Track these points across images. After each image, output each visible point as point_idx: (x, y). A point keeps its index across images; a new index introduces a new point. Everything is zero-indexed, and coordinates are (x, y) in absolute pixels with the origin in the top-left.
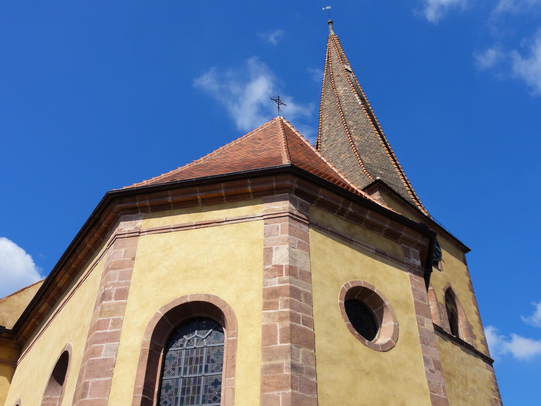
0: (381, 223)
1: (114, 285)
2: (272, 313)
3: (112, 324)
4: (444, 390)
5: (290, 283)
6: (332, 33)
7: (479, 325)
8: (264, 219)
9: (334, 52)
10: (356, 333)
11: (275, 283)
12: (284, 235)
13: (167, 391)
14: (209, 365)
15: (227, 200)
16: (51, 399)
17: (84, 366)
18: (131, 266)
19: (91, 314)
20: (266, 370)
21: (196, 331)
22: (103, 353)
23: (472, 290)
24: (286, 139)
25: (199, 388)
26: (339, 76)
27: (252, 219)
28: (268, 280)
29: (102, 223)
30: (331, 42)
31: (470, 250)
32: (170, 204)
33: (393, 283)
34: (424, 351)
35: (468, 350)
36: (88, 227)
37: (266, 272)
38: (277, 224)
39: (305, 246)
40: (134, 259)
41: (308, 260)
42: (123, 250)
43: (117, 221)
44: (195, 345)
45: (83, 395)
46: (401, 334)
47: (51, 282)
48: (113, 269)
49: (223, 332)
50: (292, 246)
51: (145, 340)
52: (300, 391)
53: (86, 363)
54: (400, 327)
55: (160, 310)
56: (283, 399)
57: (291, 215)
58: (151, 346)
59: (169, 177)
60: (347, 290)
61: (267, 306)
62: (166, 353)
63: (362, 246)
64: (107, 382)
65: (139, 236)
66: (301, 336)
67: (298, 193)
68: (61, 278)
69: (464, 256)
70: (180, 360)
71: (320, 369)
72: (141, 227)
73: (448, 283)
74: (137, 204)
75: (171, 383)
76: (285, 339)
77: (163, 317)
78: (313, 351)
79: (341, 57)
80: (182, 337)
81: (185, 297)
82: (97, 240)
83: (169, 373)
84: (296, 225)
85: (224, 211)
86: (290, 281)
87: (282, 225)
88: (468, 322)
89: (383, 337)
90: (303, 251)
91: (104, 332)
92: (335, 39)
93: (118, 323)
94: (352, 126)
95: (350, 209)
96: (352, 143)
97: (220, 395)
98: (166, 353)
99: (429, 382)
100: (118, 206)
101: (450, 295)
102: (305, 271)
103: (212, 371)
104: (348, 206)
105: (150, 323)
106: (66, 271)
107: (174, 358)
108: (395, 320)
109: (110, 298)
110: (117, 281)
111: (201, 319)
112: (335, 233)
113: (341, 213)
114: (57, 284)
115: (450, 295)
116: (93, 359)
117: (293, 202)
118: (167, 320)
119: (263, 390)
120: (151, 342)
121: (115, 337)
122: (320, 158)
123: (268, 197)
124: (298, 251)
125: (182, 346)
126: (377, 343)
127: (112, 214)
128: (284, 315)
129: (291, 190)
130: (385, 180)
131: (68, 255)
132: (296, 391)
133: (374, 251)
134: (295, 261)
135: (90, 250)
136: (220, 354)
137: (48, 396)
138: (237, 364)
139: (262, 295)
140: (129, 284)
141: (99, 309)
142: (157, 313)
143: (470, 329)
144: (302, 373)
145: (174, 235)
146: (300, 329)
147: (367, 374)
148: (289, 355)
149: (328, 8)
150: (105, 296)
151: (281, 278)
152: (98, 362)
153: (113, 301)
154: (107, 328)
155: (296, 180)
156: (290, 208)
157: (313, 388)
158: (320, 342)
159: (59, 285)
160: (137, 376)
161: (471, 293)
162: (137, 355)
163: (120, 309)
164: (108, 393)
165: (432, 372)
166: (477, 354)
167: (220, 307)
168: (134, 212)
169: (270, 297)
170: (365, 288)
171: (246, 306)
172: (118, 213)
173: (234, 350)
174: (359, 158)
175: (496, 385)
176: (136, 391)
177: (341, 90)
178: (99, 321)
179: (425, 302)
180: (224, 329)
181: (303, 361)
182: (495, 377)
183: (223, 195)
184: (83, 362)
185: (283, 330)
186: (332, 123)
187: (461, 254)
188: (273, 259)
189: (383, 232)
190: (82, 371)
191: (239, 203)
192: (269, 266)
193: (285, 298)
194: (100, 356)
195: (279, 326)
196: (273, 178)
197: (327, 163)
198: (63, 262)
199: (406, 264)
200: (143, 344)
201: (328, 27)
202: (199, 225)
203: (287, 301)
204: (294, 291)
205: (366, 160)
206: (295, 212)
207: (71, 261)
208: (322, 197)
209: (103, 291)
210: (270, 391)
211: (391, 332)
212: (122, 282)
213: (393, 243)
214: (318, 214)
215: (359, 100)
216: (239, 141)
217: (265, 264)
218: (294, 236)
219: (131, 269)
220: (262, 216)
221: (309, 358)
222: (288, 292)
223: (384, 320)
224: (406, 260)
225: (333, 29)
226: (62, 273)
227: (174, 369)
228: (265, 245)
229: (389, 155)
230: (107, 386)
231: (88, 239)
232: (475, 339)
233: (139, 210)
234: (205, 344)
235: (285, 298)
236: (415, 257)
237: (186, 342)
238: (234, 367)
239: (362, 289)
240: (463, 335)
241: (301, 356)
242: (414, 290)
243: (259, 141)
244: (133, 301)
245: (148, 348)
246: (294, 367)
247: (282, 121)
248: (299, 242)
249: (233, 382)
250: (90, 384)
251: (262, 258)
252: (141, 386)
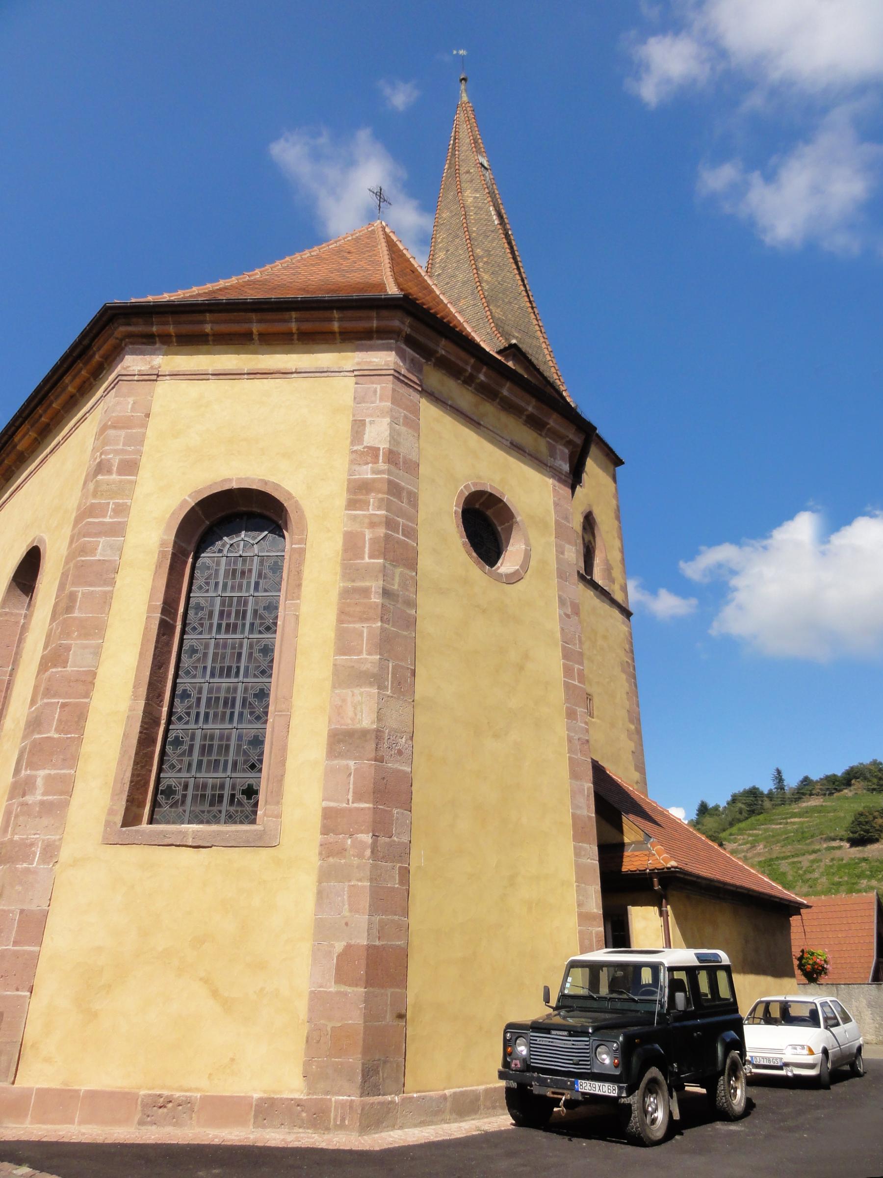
0: (523, 404)
1: (116, 452)
2: (359, 515)
3: (114, 510)
4: (580, 641)
5: (389, 474)
6: (465, 98)
7: (620, 565)
8: (355, 376)
9: (464, 129)
10: (474, 554)
11: (366, 472)
12: (383, 404)
13: (196, 614)
14: (261, 581)
15: (298, 340)
16: (12, 614)
17: (69, 569)
18: (144, 426)
19: (78, 493)
20: (346, 593)
21: (243, 532)
22: (99, 551)
23: (618, 518)
24: (392, 259)
25: (245, 612)
26: (468, 172)
27: (337, 374)
28: (357, 468)
29: (94, 354)
30: (462, 114)
31: (623, 463)
32: (207, 335)
33: (529, 491)
34: (561, 588)
35: (603, 597)
36: (70, 359)
37: (354, 456)
38: (375, 386)
39: (413, 424)
40: (148, 415)
41: (417, 445)
42: (131, 400)
43: (119, 354)
44: (241, 552)
45: (69, 609)
46: (533, 563)
47: (6, 442)
48: (114, 427)
49: (284, 537)
50: (394, 421)
51: (165, 537)
52: (393, 626)
53: (72, 565)
54: (533, 553)
55: (190, 496)
56: (369, 633)
57: (396, 374)
58: (174, 546)
59: (205, 293)
60: (467, 494)
61: (352, 504)
62: (196, 558)
63: (491, 433)
64: (105, 593)
65: (156, 380)
66: (398, 551)
67: (410, 341)
68: (24, 436)
69: (614, 470)
70: (217, 571)
71: (421, 599)
72: (160, 367)
73: (590, 506)
74: (154, 329)
75: (202, 602)
76: (377, 553)
77: (193, 508)
78: (414, 574)
79: (476, 142)
80: (221, 539)
81: (230, 480)
82: (84, 382)
83: (200, 588)
84: (403, 390)
85: (294, 357)
86: (389, 472)
87: (382, 388)
88: (607, 560)
89: (507, 564)
90: (410, 431)
91: (99, 519)
92: (469, 109)
93: (122, 510)
94: (482, 257)
95: (482, 377)
96: (478, 284)
97: (275, 624)
98: (196, 558)
99: (562, 629)
100: (123, 329)
101: (589, 522)
102: (411, 460)
103: (266, 591)
104: (479, 371)
105: (173, 513)
106: (32, 427)
107: (208, 568)
108: (527, 544)
109: (109, 472)
110: (120, 447)
111: (250, 515)
112: (457, 410)
113: (468, 381)
114: (15, 446)
115: (589, 522)
116: (83, 559)
117: (401, 354)
118: (200, 512)
119: (340, 621)
120: (175, 542)
121: (118, 530)
122: (438, 297)
123: (363, 342)
124: (403, 429)
125: (220, 551)
126: (499, 571)
127: (112, 342)
128: (376, 520)
129: (399, 336)
130: (524, 347)
131: (36, 400)
132: (387, 626)
133: (508, 444)
134: (398, 443)
135: (72, 396)
136: (277, 568)
137: (7, 610)
138: (304, 583)
139: (345, 487)
140: (140, 453)
141: (91, 486)
142: (185, 501)
143: (608, 569)
144: (397, 601)
145: (213, 385)
146: (399, 542)
147: (484, 611)
148: (381, 575)
149: (462, 52)
150: (101, 468)
151: (375, 466)
152: (92, 563)
153: (114, 477)
154: (105, 516)
155: (408, 320)
156: (395, 363)
157: (411, 623)
158: (425, 562)
159: (19, 448)
160: (153, 588)
161: (616, 523)
162: (154, 558)
163: (127, 489)
164: (107, 610)
165: (568, 616)
166: (613, 602)
167: (282, 500)
168: (148, 341)
169: (358, 492)
170: (491, 495)
171: (320, 502)
172: (121, 340)
173: (300, 562)
174: (487, 309)
175: (631, 644)
176: (150, 609)
177: (469, 196)
178: (92, 505)
179: (569, 522)
180: (285, 532)
181: (399, 585)
182: (631, 634)
183: (294, 330)
184: (67, 562)
185: (373, 541)
186: (452, 249)
187: (611, 467)
188: (366, 437)
189: (524, 417)
190: (65, 576)
191: (316, 347)
192: (359, 448)
193: (380, 496)
194: (95, 556)
195: (368, 535)
196: (374, 314)
197: (449, 305)
198: (27, 412)
199: (550, 467)
200: (163, 544)
201: (459, 89)
202: (253, 374)
203: (382, 499)
204: (392, 487)
205: (498, 313)
206: (403, 371)
207: (40, 410)
208: (443, 352)
209: (98, 460)
210: (349, 622)
211: (520, 559)
212: (128, 448)
213: (535, 435)
214: (435, 378)
215: (495, 217)
216: (315, 251)
217: (353, 443)
218: (399, 405)
219: (143, 430)
220: (353, 371)
221: (408, 582)
222: (385, 487)
223: (511, 541)
224: (550, 461)
225: (466, 90)
226: (25, 429)
227: (207, 584)
228: (354, 416)
229: (530, 310)
230: (106, 600)
231: (70, 378)
232: (614, 583)
233: (157, 339)
234: (256, 552)
235: (380, 496)
236: (563, 459)
237: (228, 546)
238: (299, 586)
239: (485, 497)
240: (598, 576)
241: (397, 579)
242: (556, 504)
243: (348, 256)
244: (146, 480)
245: (170, 549)
246: (386, 593)
247: (383, 228)
248: (406, 417)
249: (297, 607)
250: (80, 595)
251: (349, 434)
252: (159, 603)
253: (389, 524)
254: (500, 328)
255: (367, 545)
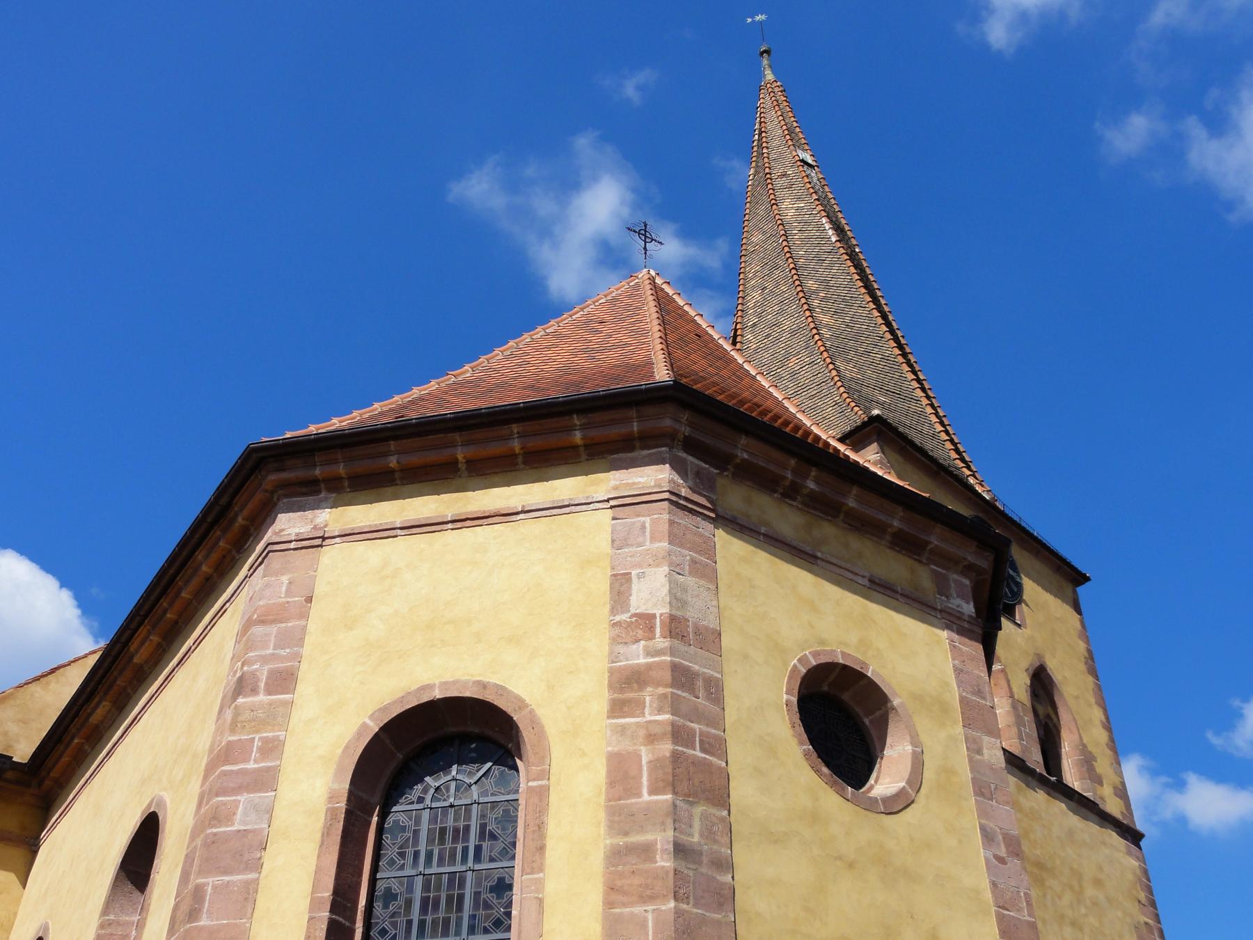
0: (882, 517)
1: (264, 660)
2: (629, 724)
3: (260, 749)
4: (1029, 904)
5: (672, 655)
6: (769, 76)
7: (1109, 752)
8: (612, 507)
9: (773, 120)
10: (825, 770)
11: (637, 655)
12: (657, 545)
13: (386, 906)
14: (485, 845)
15: (525, 463)
16: (118, 923)
17: (195, 848)
18: (305, 615)
19: (211, 726)
20: (616, 856)
21: (455, 767)
22: (238, 816)
23: (1093, 671)
24: (664, 323)
25: (461, 898)
26: (784, 175)
27: (584, 507)
28: (621, 649)
29: (236, 516)
30: (768, 98)
31: (1088, 579)
32: (393, 471)
33: (911, 656)
34: (982, 813)
35: (1084, 810)
36: (204, 526)
37: (617, 630)
38: (642, 519)
39: (706, 570)
40: (309, 599)
41: (715, 603)
42: (285, 579)
43: (270, 511)
44: (452, 800)
45: (193, 914)
46: (929, 774)
47: (119, 653)
48: (262, 622)
49: (517, 770)
50: (676, 570)
51: (336, 786)
52: (696, 905)
53: (199, 841)
54: (926, 758)
55: (371, 717)
56: (656, 923)
57: (674, 498)
58: (349, 800)
59: (390, 410)
60: (804, 671)
61: (618, 708)
62: (383, 816)
63: (838, 570)
64: (247, 883)
65: (321, 546)
66: (697, 777)
67: (691, 446)
68: (142, 643)
69: (1075, 592)
70: (416, 833)
71: (741, 855)
72: (326, 526)
73: (1039, 656)
74: (317, 472)
75: (396, 887)
76: (661, 784)
77: (376, 734)
78: (725, 813)
79: (791, 131)
80: (421, 780)
81: (429, 687)
82: (224, 557)
83: (392, 863)
84: (686, 520)
85: (519, 489)
86: (673, 651)
87: (653, 522)
88: (1084, 746)
89: (886, 780)
90: (702, 582)
91: (241, 768)
92: (776, 90)
93: (273, 748)
94: (816, 292)
95: (811, 485)
96: (815, 331)
97: (509, 914)
98: (383, 816)
99: (994, 885)
100: (273, 477)
101: (1042, 684)
102: (707, 628)
103: (492, 860)
104: (806, 477)
105: (347, 747)
107: (403, 829)
108: (915, 742)
109: (254, 691)
110: (270, 651)
111: (465, 738)
112: (776, 540)
113: (790, 493)
114: (131, 658)
115: (1042, 684)
116: (215, 830)
117: (678, 467)
118: (388, 741)
119: (609, 904)
120: (351, 793)
121: (266, 781)
122: (741, 367)
123: (621, 455)
124: (690, 581)
125: (421, 800)
126: (874, 793)
127: (259, 496)
128: (657, 730)
129: (673, 440)
130: (891, 417)
131: (158, 590)
132: (685, 906)
133: (866, 582)
134: (684, 604)
135: (208, 579)
136: (509, 818)
137: (112, 917)
138: (550, 844)
139: (606, 682)
140: (298, 658)
141: (229, 714)
142: (364, 725)
143: (1088, 761)
144: (700, 863)
145: (402, 544)
146: (696, 762)
147: (851, 865)
148: (669, 821)
149: (759, 18)
150: (242, 686)
151: (651, 643)
152: (227, 837)
153: (262, 698)
154: (247, 760)
155: (685, 416)
156: (671, 481)
157: (726, 898)
158: (742, 791)
159: (136, 660)
160: (318, 870)
161: (1091, 679)
162: (317, 823)
163: (278, 716)
164: (250, 911)
165: (1001, 860)
166: (1105, 819)
167: (509, 711)
168: (310, 491)
169: (626, 687)
170: (845, 667)
171: (569, 708)
172: (273, 492)
173: (541, 811)
174: (831, 366)
175: (1150, 891)
176: (314, 904)
177: (789, 208)
178: (229, 743)
179: (984, 698)
180: (518, 761)
181: (701, 835)
182: (1145, 872)
183: (517, 451)
184: (193, 837)
185: (655, 765)
186: (770, 286)
187: (1068, 589)
188: (633, 599)
189: (888, 537)
190: (189, 859)
191: (553, 470)
192: (624, 617)
193: (661, 690)
194: (233, 824)
195: (646, 756)
196: (633, 413)
197: (758, 377)
198: (146, 607)
199: (941, 611)
200: (332, 797)
201: (760, 63)
202: (460, 522)
203: (664, 696)
204: (681, 675)
205: (848, 370)
206: (684, 492)
207: (164, 603)
208: (745, 456)
209: (238, 674)
210: (624, 905)
211: (905, 768)
212: (282, 652)
213: (910, 562)
214: (736, 496)
215: (830, 232)
216: (552, 326)
217: (613, 611)
218: (681, 545)
219: (303, 623)
220: (607, 501)
221: (715, 829)
222: (667, 676)
223: (889, 741)
224: (940, 601)
225: (770, 66)
226: (145, 632)
227: (402, 855)
228: (613, 568)
229: (901, 359)
230: (249, 894)
231: (203, 553)
232: (1101, 784)
233: (323, 486)
234: (475, 797)
235: (661, 690)
236: (961, 596)
237: (432, 791)
238: (542, 849)
239: (837, 670)
240: (1072, 776)
241: (697, 824)
242: (958, 671)
243: (600, 327)
244: (307, 698)
245: (342, 805)
246: (680, 850)
247: (652, 280)
248: (693, 561)
249: (540, 884)
250: (210, 889)
251: (607, 598)
252: (327, 894)
253: (679, 734)
254: (854, 391)
255: (645, 768)
